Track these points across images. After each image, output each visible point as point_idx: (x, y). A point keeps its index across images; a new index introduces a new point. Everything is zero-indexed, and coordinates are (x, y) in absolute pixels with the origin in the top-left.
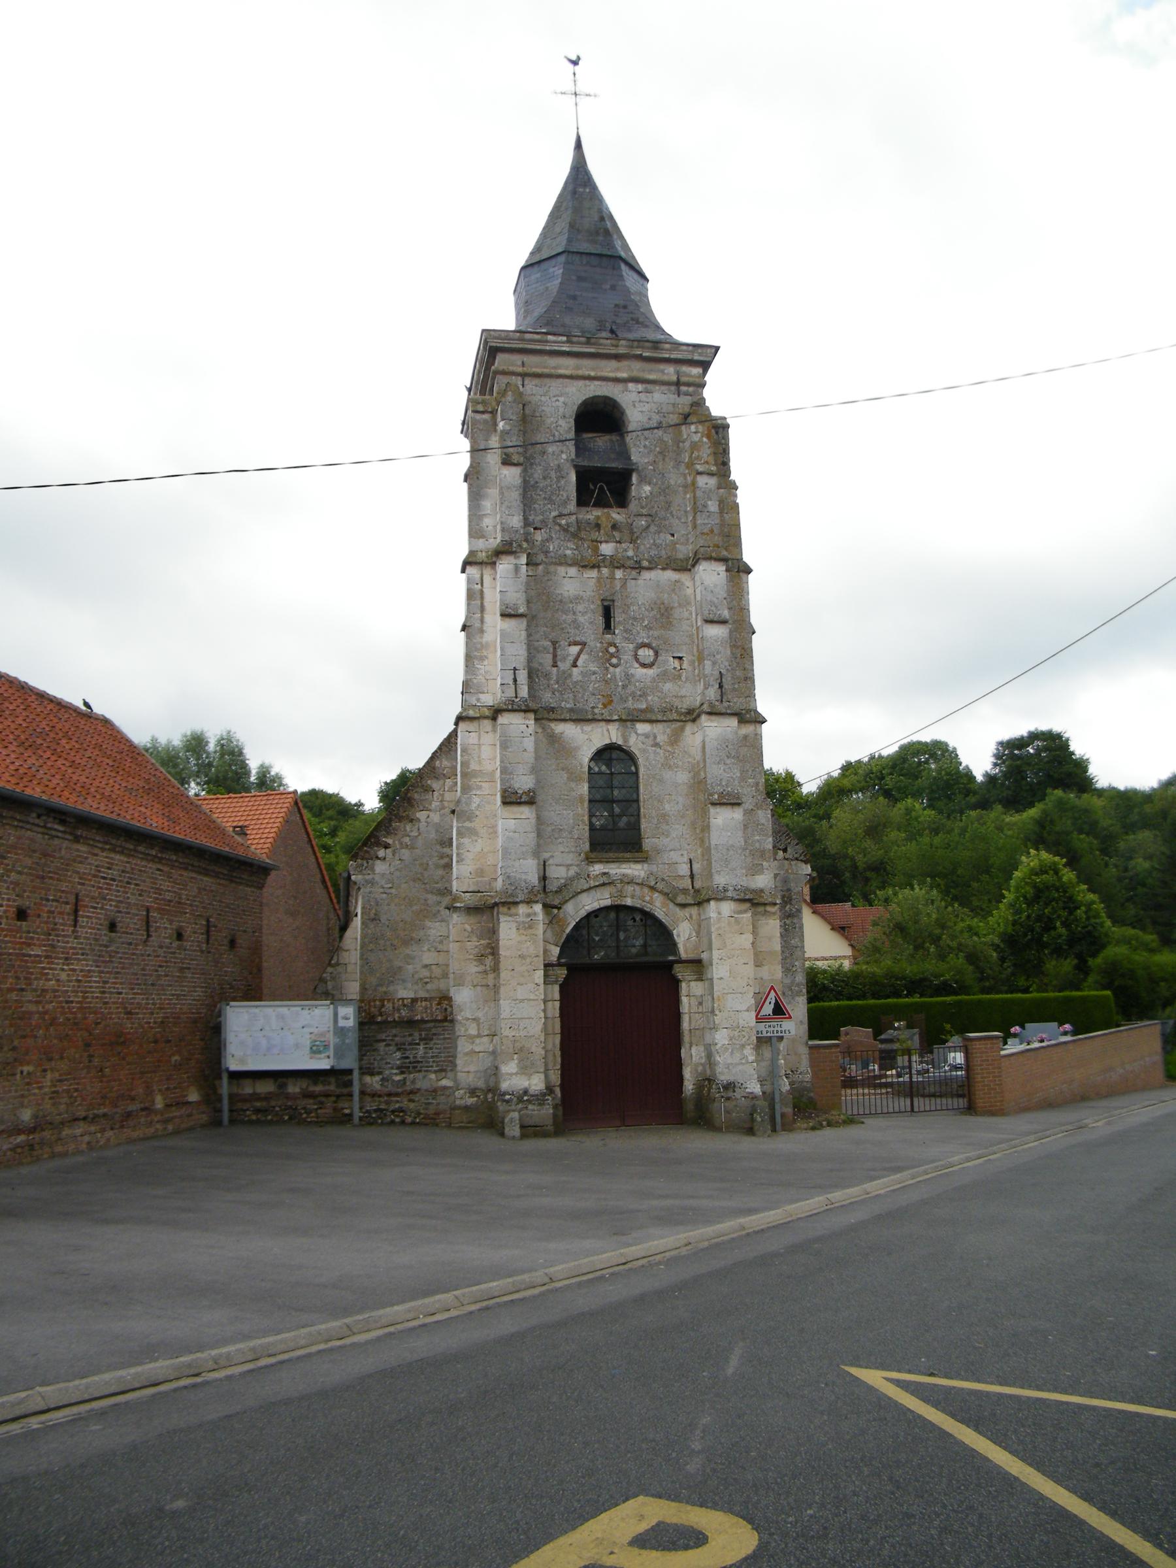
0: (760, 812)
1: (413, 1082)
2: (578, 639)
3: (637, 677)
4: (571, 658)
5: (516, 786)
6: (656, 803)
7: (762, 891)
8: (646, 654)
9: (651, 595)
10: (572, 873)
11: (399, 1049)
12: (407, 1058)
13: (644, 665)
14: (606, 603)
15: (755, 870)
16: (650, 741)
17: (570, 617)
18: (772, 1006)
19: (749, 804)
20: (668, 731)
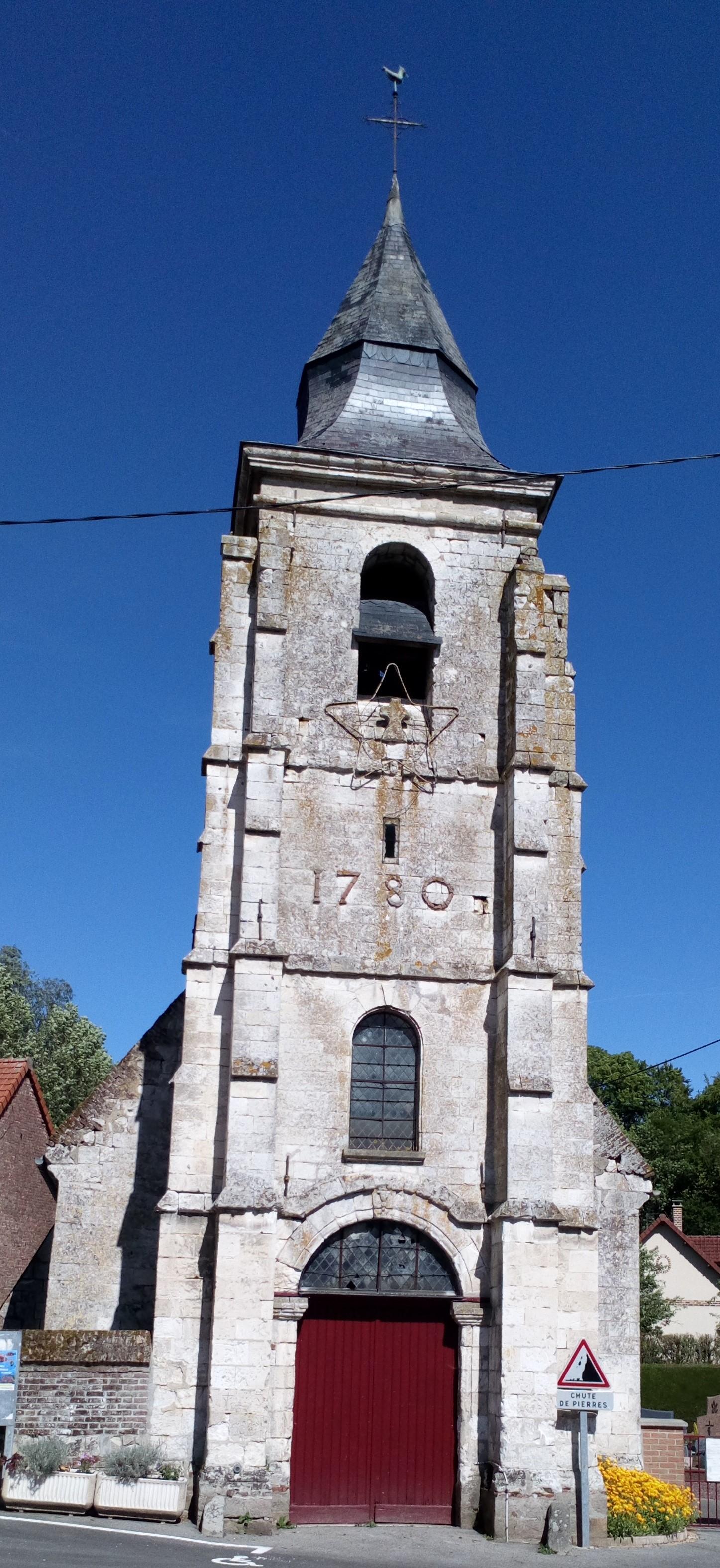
0: (578, 1105)
1: (89, 1447)
2: (349, 868)
3: (425, 921)
4: (340, 892)
5: (253, 1055)
6: (439, 1086)
7: (576, 1211)
8: (437, 892)
9: (450, 813)
10: (323, 1174)
11: (73, 1401)
12: (84, 1413)
13: (434, 907)
14: (389, 823)
15: (571, 1182)
16: (437, 1005)
17: (341, 840)
18: (582, 1368)
19: (561, 1092)
20: (460, 993)
